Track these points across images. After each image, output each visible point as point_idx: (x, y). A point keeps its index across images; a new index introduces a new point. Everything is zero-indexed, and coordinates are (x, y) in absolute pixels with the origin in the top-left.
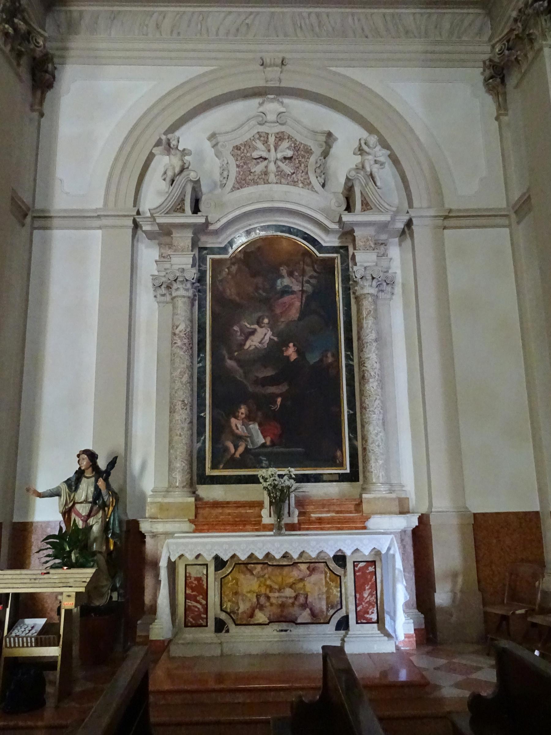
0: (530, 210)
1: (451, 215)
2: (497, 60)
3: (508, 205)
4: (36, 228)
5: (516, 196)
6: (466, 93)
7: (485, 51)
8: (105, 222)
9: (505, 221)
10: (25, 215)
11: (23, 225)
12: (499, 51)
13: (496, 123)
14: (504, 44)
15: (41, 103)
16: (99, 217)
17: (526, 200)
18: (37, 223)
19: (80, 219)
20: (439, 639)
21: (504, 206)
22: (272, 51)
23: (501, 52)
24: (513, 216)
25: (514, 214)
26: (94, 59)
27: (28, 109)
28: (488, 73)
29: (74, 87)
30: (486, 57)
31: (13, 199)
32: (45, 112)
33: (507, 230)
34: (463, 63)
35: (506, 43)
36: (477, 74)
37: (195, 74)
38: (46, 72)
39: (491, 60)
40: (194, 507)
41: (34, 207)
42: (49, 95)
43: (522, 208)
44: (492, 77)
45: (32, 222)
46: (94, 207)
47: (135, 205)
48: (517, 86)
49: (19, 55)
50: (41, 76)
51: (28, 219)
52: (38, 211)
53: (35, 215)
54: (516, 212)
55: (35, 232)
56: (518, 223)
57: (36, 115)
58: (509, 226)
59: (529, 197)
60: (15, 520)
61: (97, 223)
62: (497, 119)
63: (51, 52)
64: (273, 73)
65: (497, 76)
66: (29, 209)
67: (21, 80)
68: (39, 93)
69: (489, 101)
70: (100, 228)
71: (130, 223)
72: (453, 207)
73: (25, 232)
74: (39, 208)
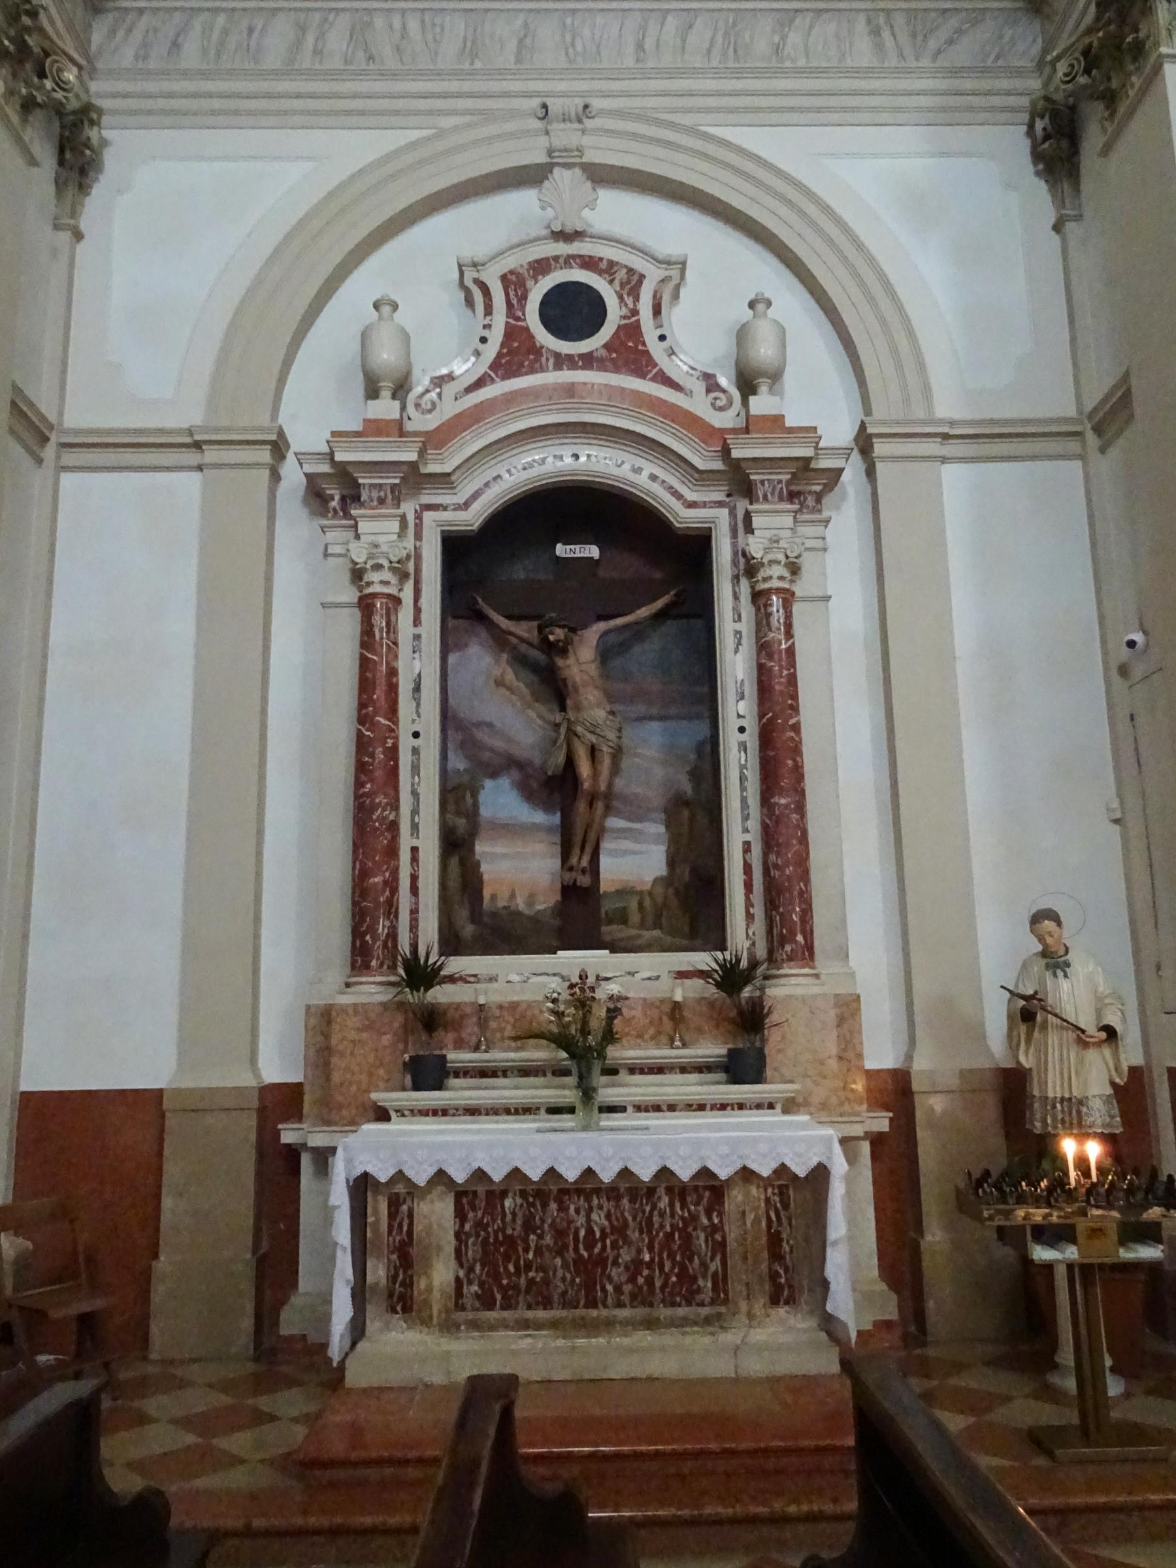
2: (1059, 97)
3: (1080, 411)
4: (66, 469)
6: (993, 171)
9: (1073, 446)
11: (39, 461)
13: (1056, 239)
15: (74, 214)
18: (69, 458)
21: (1072, 412)
23: (1070, 77)
24: (1090, 436)
27: (48, 229)
29: (141, 167)
31: (14, 404)
32: (84, 225)
33: (1078, 464)
35: (1082, 59)
36: (1013, 143)
37: (402, 142)
39: (1047, 99)
41: (61, 423)
43: (1111, 417)
45: (58, 457)
49: (28, 106)
50: (76, 157)
51: (49, 452)
54: (1098, 430)
56: (1103, 450)
58: (1082, 457)
60: (24, 1087)
62: (1057, 228)
63: (98, 102)
65: (1058, 147)
66: (51, 427)
67: (33, 162)
68: (71, 191)
73: (38, 479)
74: (72, 426)
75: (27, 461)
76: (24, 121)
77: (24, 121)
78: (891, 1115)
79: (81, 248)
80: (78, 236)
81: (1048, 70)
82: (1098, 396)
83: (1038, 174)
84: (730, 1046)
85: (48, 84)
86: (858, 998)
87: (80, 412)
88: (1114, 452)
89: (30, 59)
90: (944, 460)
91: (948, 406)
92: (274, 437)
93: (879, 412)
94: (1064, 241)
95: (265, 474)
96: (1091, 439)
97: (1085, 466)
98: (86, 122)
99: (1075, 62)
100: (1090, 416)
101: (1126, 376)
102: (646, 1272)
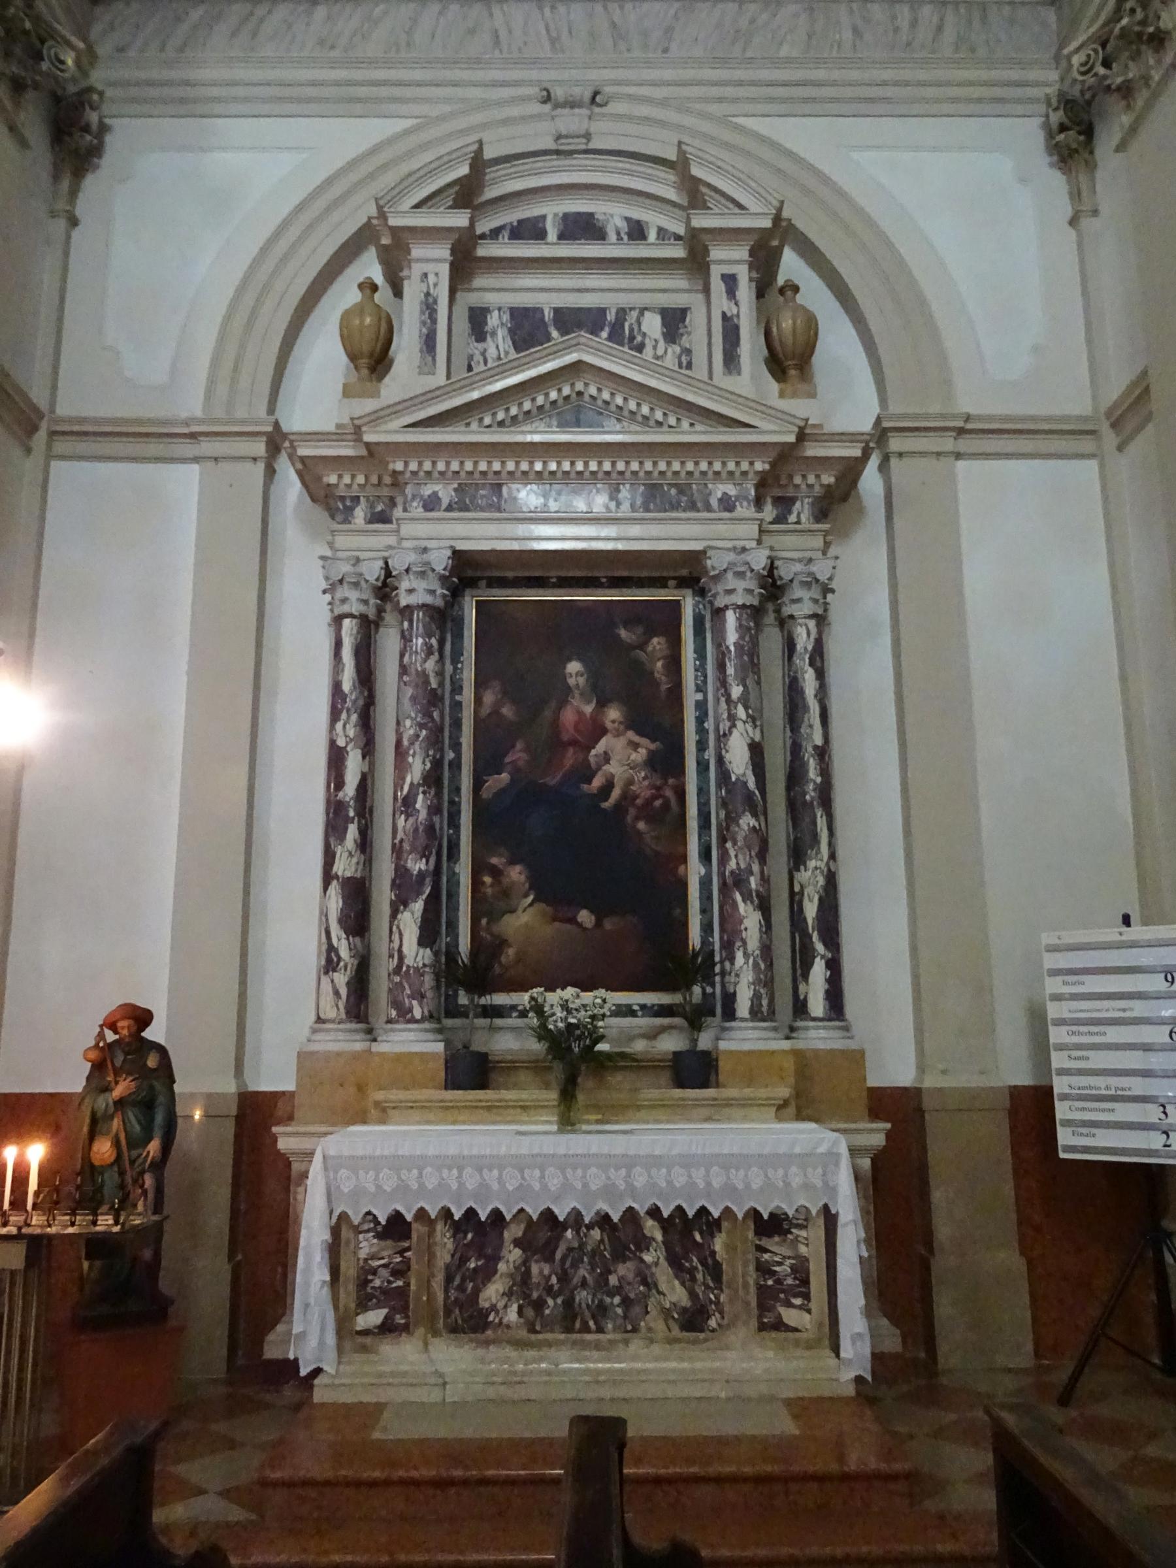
0: (1149, 418)
1: (969, 426)
3: (1096, 409)
5: (1115, 387)
7: (1047, 80)
8: (207, 447)
9: (1087, 445)
10: (35, 428)
11: (29, 451)
12: (1082, 65)
14: (1095, 51)
15: (74, 193)
16: (193, 436)
17: (1139, 399)
18: (60, 446)
19: (145, 439)
20: (940, 1367)
22: (571, 79)
25: (1111, 431)
26: (187, 103)
28: (1056, 117)
30: (1052, 91)
33: (1093, 464)
34: (996, 104)
36: (1028, 132)
38: (86, 129)
39: (1061, 95)
40: (873, 420)
41: (53, 411)
42: (92, 184)
43: (1131, 412)
44: (1063, 128)
45: (49, 446)
46: (184, 415)
47: (271, 410)
48: (1121, 147)
50: (73, 138)
51: (42, 435)
52: (63, 420)
53: (58, 428)
54: (1114, 425)
55: (55, 465)
56: (1120, 448)
57: (62, 223)
59: (1147, 390)
61: (189, 449)
62: (1073, 222)
64: (571, 121)
65: (1075, 132)
66: (41, 416)
67: (23, 143)
69: (1057, 181)
70: (196, 460)
71: (259, 448)
72: (972, 411)
73: (31, 466)
75: (18, 452)
76: (17, 104)
77: (17, 104)
78: (888, 1126)
79: (76, 234)
80: (74, 222)
81: (1064, 63)
82: (1115, 395)
83: (1051, 165)
84: (833, 473)
85: (45, 66)
86: (862, 1053)
87: (75, 401)
88: (1133, 448)
89: (35, 43)
90: (958, 456)
91: (183, 483)
92: (270, 429)
93: (894, 408)
94: (1080, 235)
95: (261, 466)
96: (1110, 439)
97: (1102, 466)
98: (87, 107)
99: (1092, 53)
100: (1109, 414)
101: (1145, 373)
102: (747, 821)
